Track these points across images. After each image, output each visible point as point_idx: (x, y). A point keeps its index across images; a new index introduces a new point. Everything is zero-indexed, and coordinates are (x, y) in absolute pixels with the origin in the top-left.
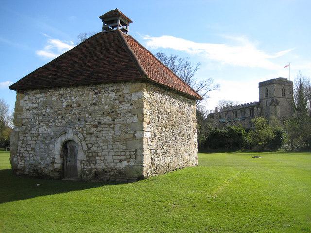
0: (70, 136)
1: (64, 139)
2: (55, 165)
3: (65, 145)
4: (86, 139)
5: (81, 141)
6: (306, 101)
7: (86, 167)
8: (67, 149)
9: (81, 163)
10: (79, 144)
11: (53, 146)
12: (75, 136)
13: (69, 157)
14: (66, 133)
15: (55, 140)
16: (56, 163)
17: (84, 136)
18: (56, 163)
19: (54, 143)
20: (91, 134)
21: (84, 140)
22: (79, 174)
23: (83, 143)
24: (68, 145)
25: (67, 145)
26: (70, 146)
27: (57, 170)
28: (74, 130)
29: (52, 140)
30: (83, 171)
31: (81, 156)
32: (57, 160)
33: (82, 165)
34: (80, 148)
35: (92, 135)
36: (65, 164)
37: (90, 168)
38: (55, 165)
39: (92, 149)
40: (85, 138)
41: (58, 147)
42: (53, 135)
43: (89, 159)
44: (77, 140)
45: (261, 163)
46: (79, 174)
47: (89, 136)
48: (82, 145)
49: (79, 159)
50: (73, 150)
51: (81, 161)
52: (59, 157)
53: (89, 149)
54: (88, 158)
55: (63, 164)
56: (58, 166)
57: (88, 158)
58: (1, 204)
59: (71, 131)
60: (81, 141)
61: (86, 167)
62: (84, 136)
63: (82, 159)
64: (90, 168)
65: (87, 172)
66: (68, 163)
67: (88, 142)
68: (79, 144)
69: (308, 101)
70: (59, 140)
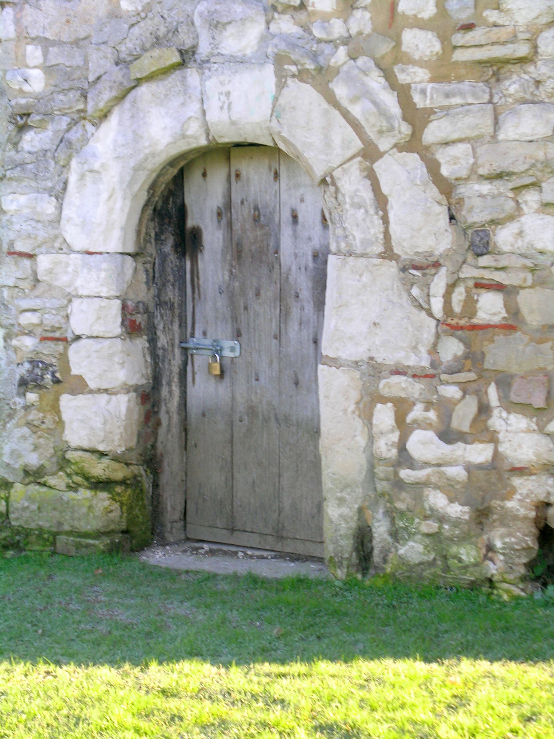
0: (238, 99)
1: (162, 125)
2: (67, 402)
3: (167, 216)
4: (433, 133)
5: (370, 154)
6: (514, 537)
7: (424, 444)
8: (188, 242)
9: (370, 400)
10: (352, 183)
11: (48, 207)
12: (304, 97)
13: (211, 327)
14: (186, 57)
15: (67, 147)
16: (80, 387)
17: (403, 94)
18: (80, 387)
19: (52, 176)
20: (494, 70)
21: (413, 144)
22: (338, 517)
23: (400, 173)
24: (204, 202)
25: (190, 199)
26: (225, 213)
27: (99, 469)
28: (286, 25)
29: (31, 141)
30: (391, 482)
31: (366, 320)
32: (82, 361)
33: (384, 416)
34: (359, 226)
35: (513, 86)
36: (170, 395)
37: (479, 453)
38: (67, 402)
39: (504, 237)
40: (416, 118)
41: (100, 212)
42: (37, 83)
43: (472, 359)
44: (316, 134)
45: (248, 325)
46: (338, 517)
47: (470, 91)
48: (381, 201)
49: (349, 352)
50: (255, 250)
51: (373, 370)
52: (113, 324)
53: (479, 243)
54: (452, 349)
55: (149, 398)
56: (97, 419)
57: (452, 349)
58: (5, 665)
59: (255, 30)
60: (370, 154)
61: (424, 444)
62: (403, 94)
63: (388, 357)
64: (479, 453)
65: (437, 500)
66: (203, 389)
67: (453, 162)
68: (352, 183)
69: (513, 540)
70: (106, 142)
